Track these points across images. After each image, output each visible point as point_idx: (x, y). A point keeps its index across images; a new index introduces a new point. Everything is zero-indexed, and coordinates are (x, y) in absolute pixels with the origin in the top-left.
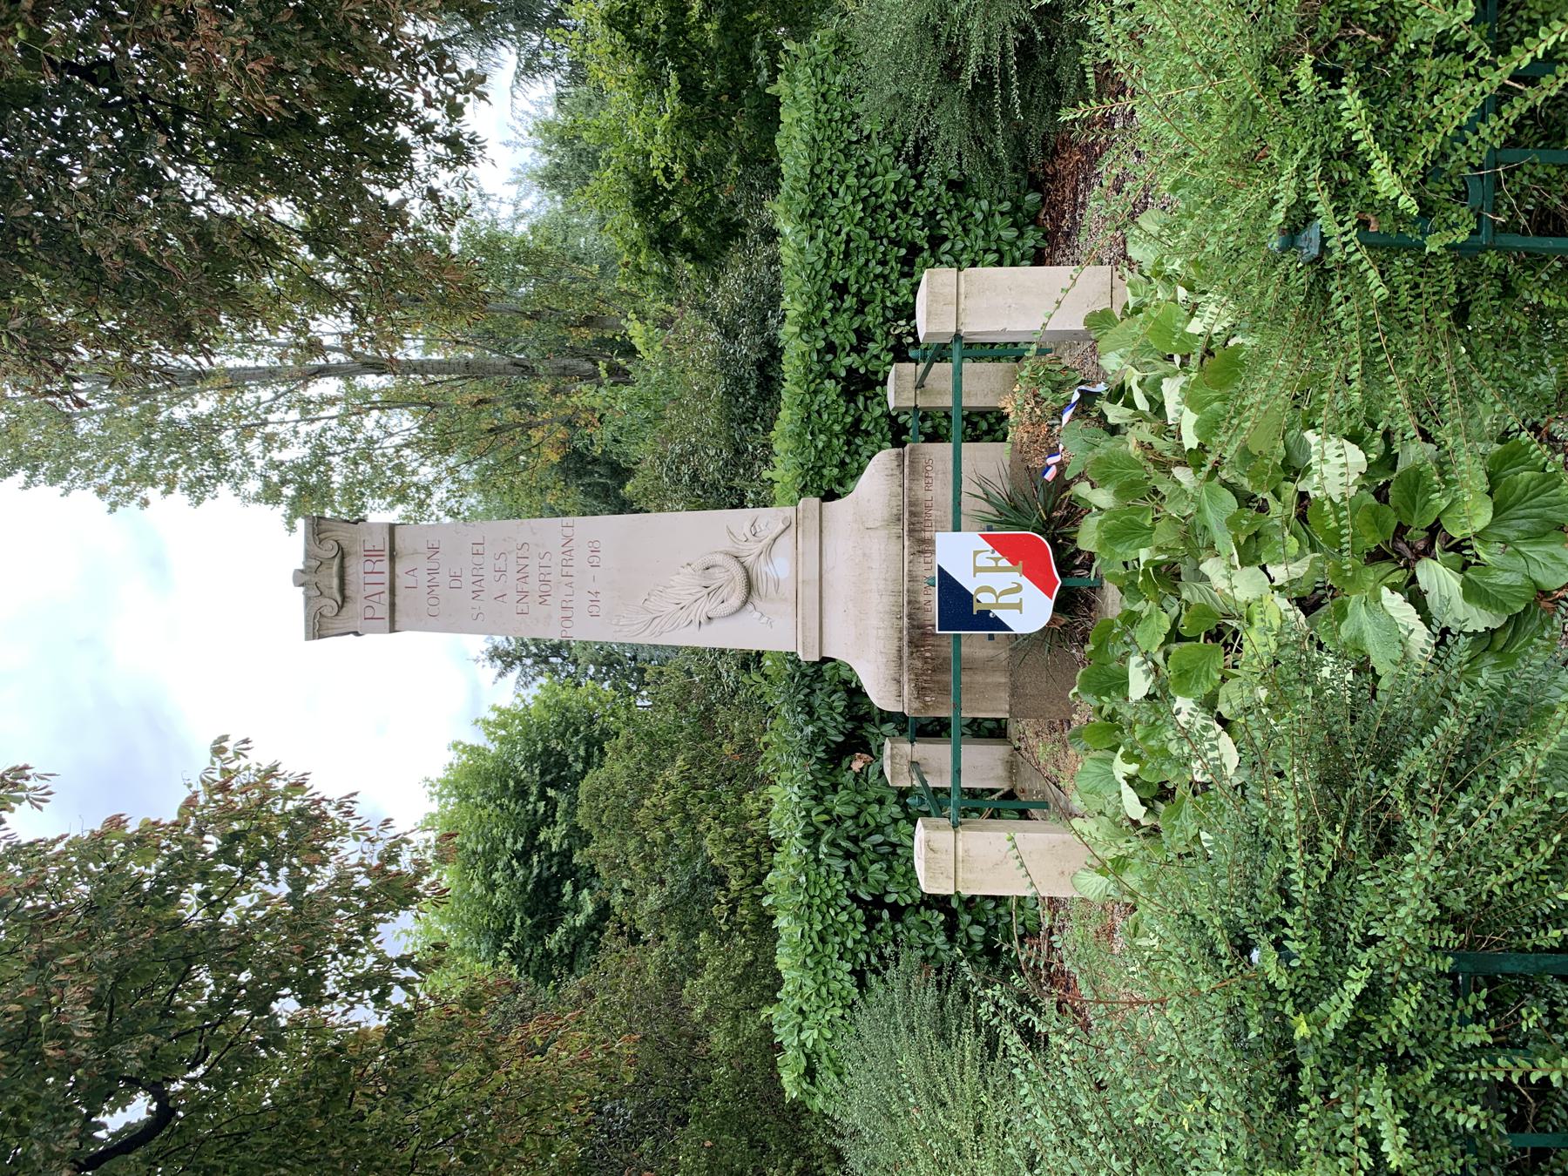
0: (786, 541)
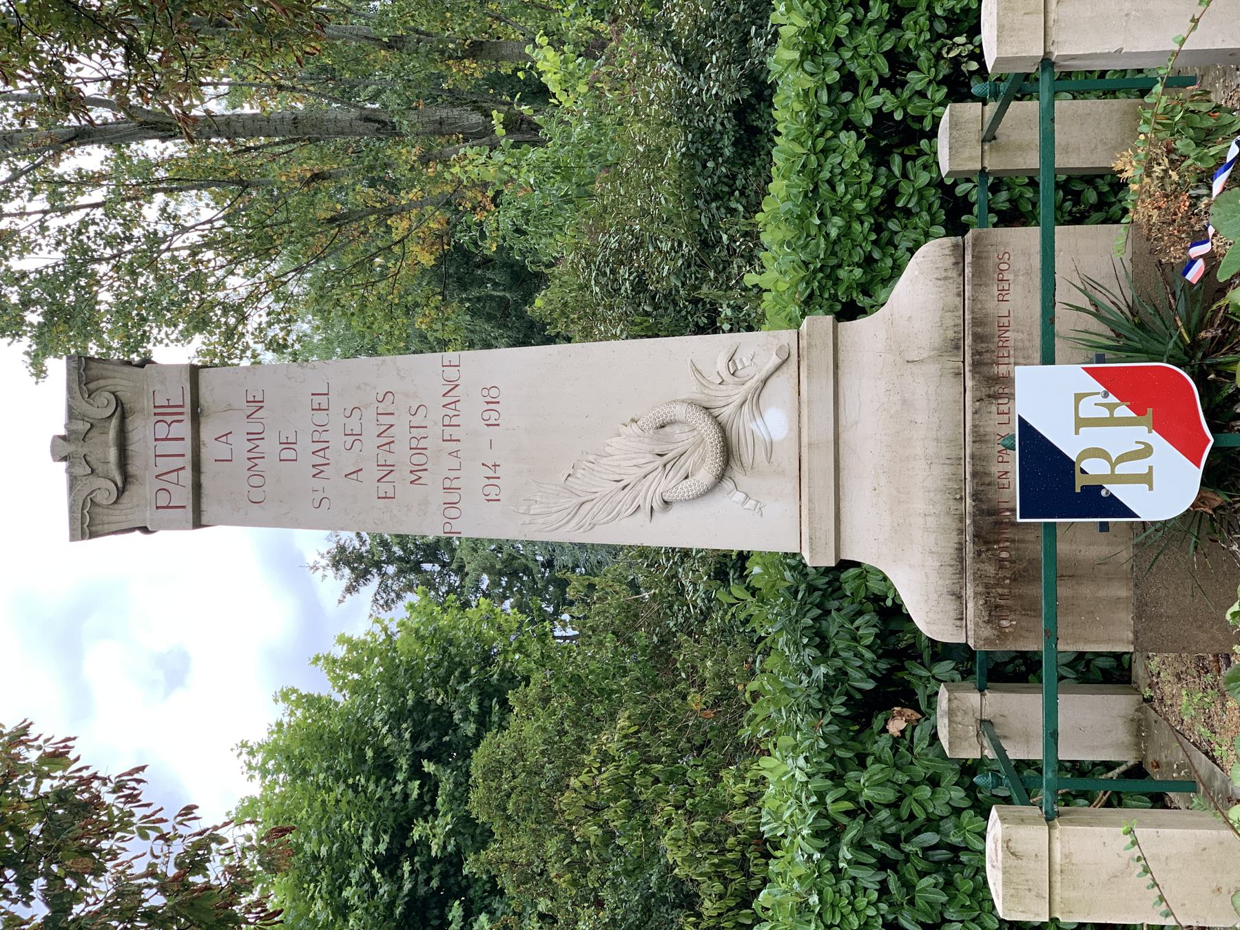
0: (783, 385)
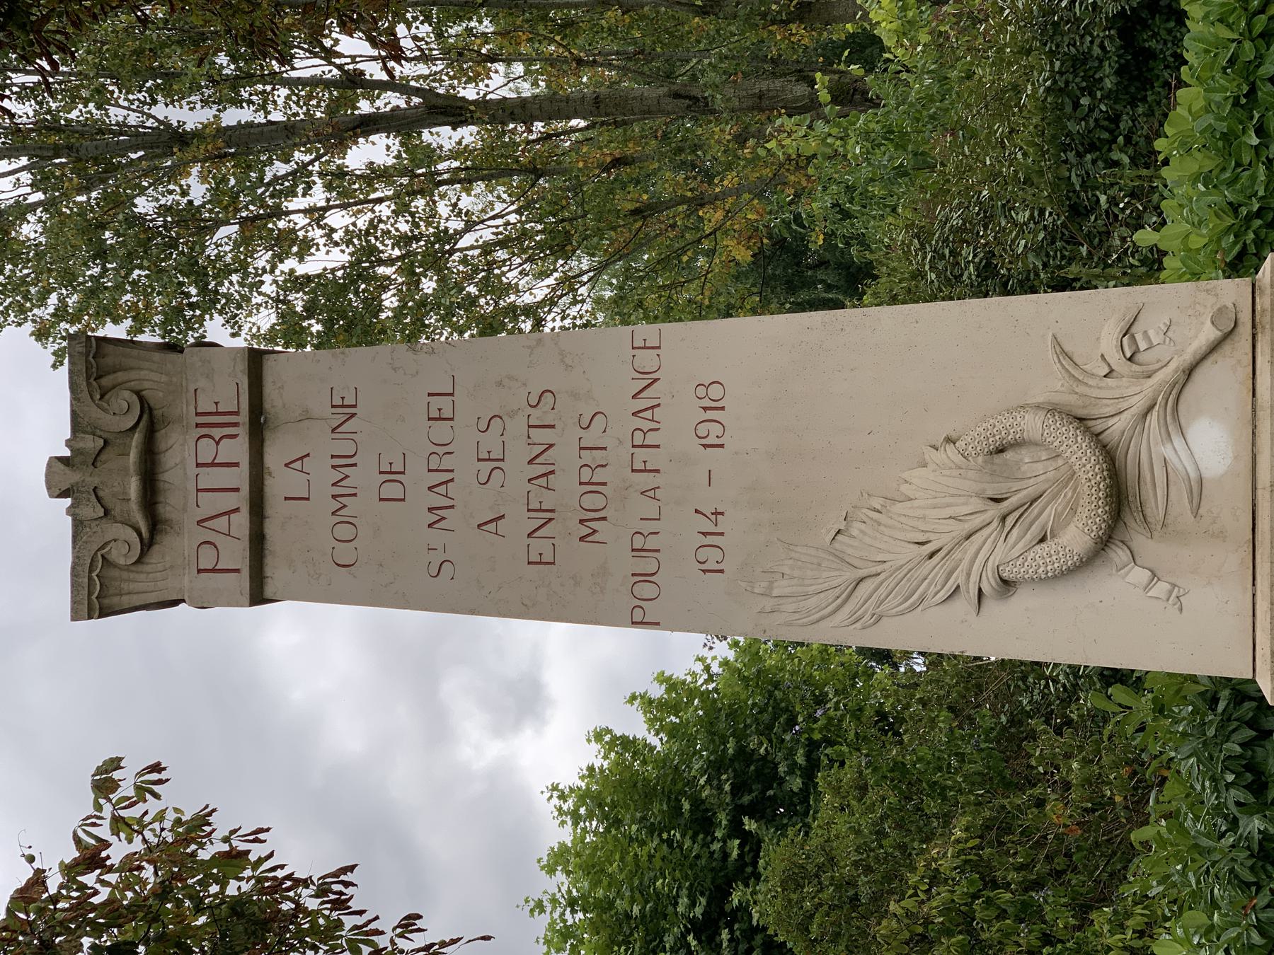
0: (1223, 377)
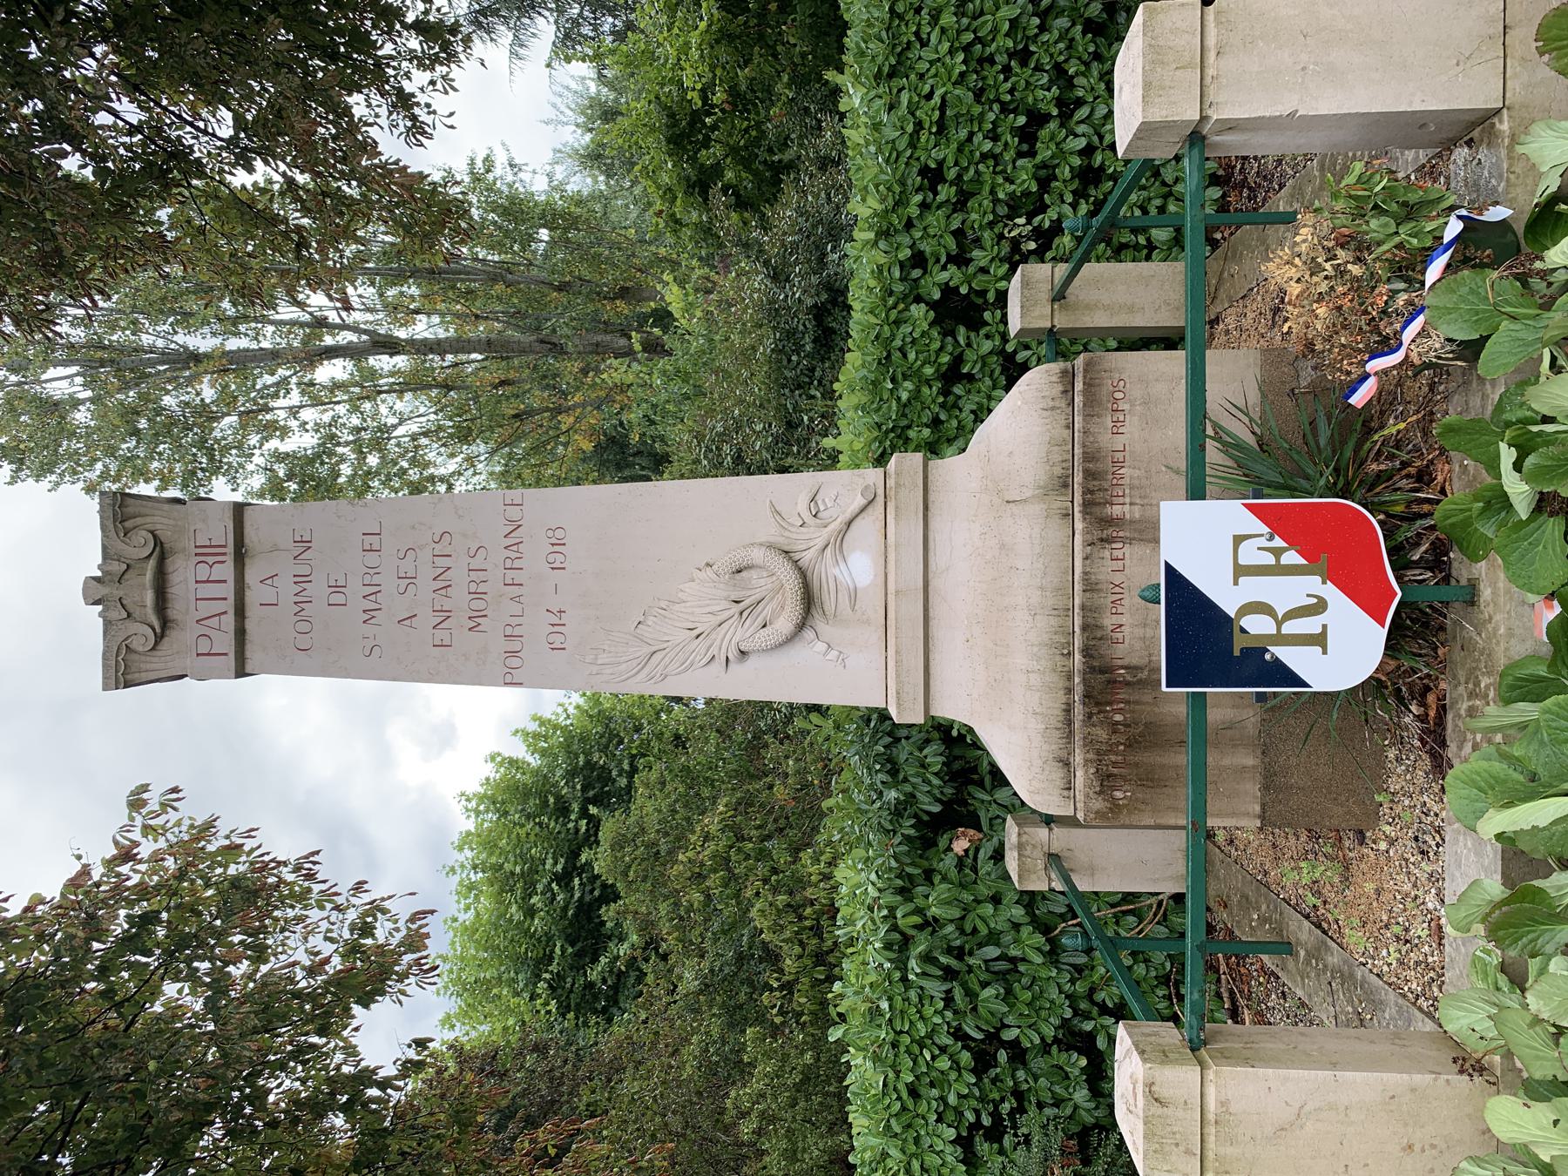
0: (868, 527)
